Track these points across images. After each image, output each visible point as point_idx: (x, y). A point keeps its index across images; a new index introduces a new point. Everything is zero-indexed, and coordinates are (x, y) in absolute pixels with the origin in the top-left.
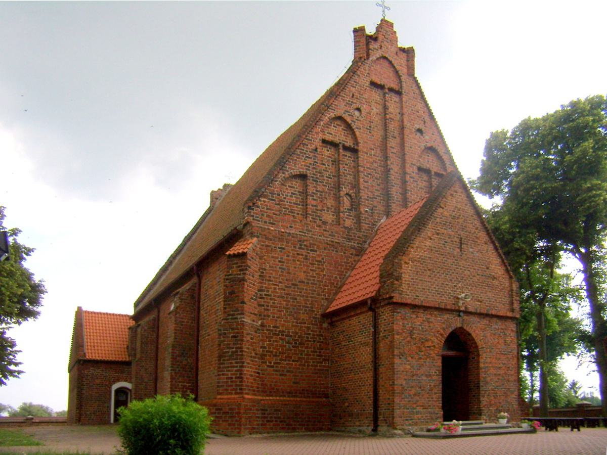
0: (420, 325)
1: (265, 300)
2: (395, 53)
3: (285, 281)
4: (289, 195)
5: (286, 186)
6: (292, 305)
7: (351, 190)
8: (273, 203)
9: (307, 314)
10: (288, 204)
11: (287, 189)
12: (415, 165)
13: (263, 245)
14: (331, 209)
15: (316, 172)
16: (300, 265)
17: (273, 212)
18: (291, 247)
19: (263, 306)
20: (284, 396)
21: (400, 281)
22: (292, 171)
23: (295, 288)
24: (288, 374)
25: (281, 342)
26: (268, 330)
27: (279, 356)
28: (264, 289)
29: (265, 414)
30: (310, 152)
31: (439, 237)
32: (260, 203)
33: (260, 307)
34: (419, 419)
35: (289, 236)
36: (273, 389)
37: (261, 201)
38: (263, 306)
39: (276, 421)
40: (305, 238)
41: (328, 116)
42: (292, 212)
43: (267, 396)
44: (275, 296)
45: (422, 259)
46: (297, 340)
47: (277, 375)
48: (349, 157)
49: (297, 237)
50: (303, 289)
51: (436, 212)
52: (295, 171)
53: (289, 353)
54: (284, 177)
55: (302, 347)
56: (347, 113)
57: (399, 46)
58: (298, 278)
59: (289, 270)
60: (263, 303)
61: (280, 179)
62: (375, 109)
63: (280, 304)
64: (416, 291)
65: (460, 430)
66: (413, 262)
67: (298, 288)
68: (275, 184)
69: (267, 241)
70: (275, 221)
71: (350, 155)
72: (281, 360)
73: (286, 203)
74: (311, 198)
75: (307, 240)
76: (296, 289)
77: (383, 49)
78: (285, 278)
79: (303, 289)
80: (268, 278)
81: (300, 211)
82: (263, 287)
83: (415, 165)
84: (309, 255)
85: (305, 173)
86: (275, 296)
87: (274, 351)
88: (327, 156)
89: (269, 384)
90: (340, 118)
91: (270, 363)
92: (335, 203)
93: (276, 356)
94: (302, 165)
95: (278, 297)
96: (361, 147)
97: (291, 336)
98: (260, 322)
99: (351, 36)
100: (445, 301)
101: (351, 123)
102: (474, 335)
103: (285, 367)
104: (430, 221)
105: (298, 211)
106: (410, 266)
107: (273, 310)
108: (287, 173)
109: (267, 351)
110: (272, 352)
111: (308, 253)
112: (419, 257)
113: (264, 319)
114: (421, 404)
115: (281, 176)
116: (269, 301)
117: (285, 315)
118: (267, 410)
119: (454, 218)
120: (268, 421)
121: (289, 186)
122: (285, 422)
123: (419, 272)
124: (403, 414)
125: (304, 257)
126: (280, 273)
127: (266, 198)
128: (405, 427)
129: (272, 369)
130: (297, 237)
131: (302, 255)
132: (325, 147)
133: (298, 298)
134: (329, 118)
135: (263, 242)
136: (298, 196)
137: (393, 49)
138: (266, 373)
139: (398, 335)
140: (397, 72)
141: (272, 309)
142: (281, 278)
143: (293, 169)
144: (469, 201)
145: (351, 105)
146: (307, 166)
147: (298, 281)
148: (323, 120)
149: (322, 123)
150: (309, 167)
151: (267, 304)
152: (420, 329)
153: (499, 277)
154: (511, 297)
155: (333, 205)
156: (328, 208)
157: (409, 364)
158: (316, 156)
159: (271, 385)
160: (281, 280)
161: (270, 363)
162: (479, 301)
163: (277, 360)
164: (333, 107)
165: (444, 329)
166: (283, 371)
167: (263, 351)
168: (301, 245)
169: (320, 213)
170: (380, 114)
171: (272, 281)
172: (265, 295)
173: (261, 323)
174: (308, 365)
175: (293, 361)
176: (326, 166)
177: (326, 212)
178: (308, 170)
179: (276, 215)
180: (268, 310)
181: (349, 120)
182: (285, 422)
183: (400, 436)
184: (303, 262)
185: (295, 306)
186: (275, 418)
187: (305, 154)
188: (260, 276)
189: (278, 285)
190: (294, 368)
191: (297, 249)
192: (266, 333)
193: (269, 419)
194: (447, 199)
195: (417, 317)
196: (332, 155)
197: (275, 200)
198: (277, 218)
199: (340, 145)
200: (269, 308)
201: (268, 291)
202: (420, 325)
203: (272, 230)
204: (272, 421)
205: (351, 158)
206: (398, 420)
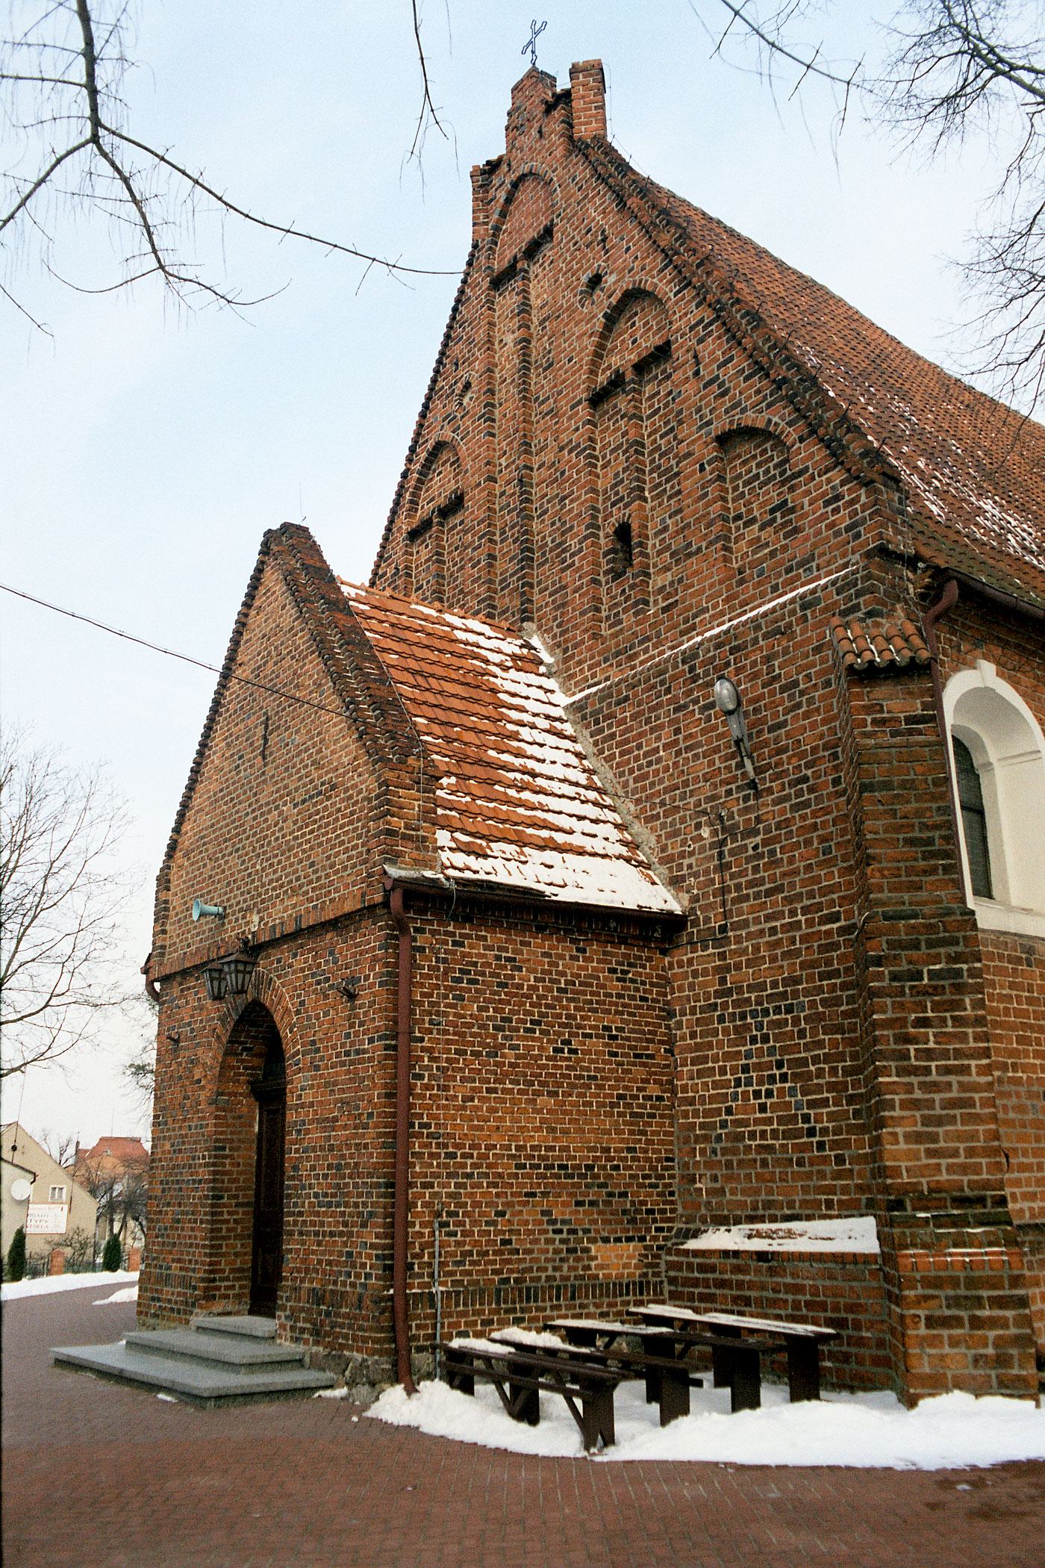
99: (468, 186)
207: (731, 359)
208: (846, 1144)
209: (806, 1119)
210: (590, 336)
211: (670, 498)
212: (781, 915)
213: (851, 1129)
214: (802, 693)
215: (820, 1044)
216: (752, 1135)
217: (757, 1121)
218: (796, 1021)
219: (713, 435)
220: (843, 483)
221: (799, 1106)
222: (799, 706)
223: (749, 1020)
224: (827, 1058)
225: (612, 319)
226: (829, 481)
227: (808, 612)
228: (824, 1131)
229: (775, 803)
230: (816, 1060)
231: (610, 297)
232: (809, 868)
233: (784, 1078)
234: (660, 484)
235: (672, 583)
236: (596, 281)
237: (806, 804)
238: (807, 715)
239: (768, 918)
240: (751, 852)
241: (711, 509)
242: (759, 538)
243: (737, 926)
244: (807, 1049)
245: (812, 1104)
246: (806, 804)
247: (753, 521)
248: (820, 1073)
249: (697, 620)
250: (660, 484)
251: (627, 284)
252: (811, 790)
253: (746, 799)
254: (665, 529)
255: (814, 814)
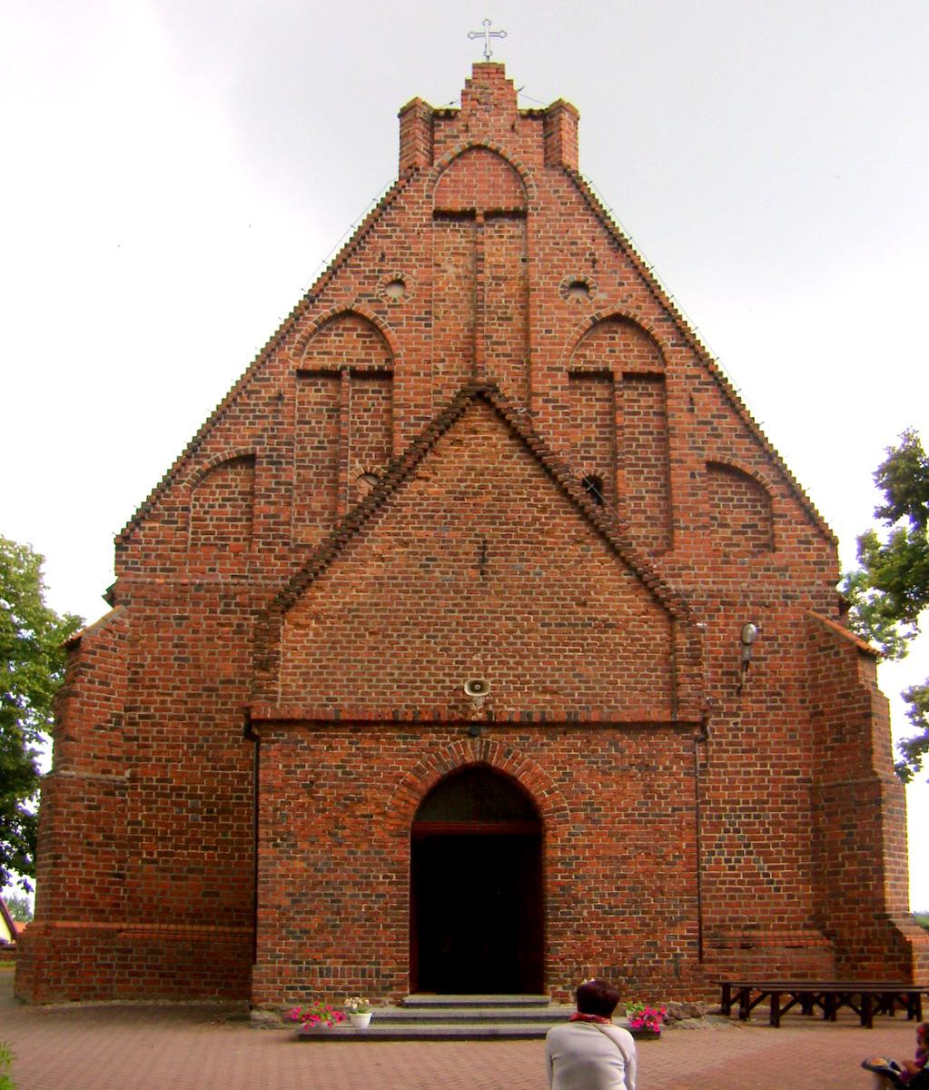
0: (338, 767)
1: (141, 727)
2: (508, 127)
3: (188, 684)
4: (217, 504)
5: (210, 486)
6: (201, 733)
7: (377, 462)
8: (171, 529)
9: (239, 747)
10: (215, 522)
11: (213, 493)
12: (560, 369)
13: (139, 618)
14: (323, 514)
15: (278, 444)
16: (224, 646)
17: (169, 546)
18: (204, 612)
19: (136, 739)
20: (182, 922)
21: (272, 670)
22: (218, 454)
23: (211, 696)
24: (191, 876)
25: (175, 810)
26: (144, 788)
27: (170, 839)
28: (138, 704)
29: (125, 959)
30: (264, 404)
31: (410, 549)
32: (142, 533)
33: (130, 743)
34: (328, 988)
35: (199, 590)
36: (156, 907)
37: (143, 529)
38: (136, 739)
39: (150, 975)
40: (239, 588)
41: (316, 317)
42: (223, 539)
43: (141, 921)
44: (163, 717)
45: (350, 610)
46: (215, 804)
47: (163, 878)
48: (373, 392)
49: (218, 591)
50: (231, 696)
51: (401, 493)
52: (226, 452)
53: (195, 833)
54: (199, 471)
55: (227, 819)
56: (364, 300)
57: (524, 104)
58: (218, 675)
59: (198, 660)
60: (135, 734)
61: (189, 477)
62: (451, 270)
63: (175, 732)
64: (327, 687)
65: (365, 1021)
66: (318, 621)
67: (217, 696)
68: (179, 489)
69: (148, 608)
70: (176, 564)
71: (377, 388)
72: (176, 847)
73: (208, 522)
74: (263, 501)
75: (242, 593)
76: (214, 699)
77: (474, 131)
78: (188, 679)
79: (231, 696)
80: (147, 683)
81: (241, 533)
82: (135, 701)
83: (560, 369)
84: (245, 623)
85: (250, 452)
86: (163, 717)
87: (160, 828)
88: (316, 403)
89: (145, 898)
90: (349, 314)
91: (150, 854)
92: (330, 501)
93: (163, 839)
94: (243, 437)
95: (171, 718)
96: (400, 364)
97: (200, 797)
98: (127, 773)
99: (395, 126)
100: (425, 700)
101: (377, 318)
102: (525, 779)
103: (185, 863)
104: (381, 516)
105: (235, 533)
106: (311, 633)
107: (159, 745)
108: (206, 461)
109: (143, 831)
110: (154, 832)
111: (245, 619)
112: (340, 607)
113: (137, 766)
114: (340, 953)
115: (192, 470)
116: (150, 728)
117: (185, 754)
118: (130, 951)
119: (461, 497)
120: (132, 974)
121: (217, 486)
122: (173, 976)
123: (340, 642)
124: (280, 974)
125: (235, 628)
126: (177, 669)
127: (155, 521)
128: (285, 1005)
129: (154, 866)
130: (218, 591)
131: (230, 625)
132: (310, 385)
133: (218, 716)
134: (316, 322)
135: (139, 611)
136: (240, 502)
137: (504, 121)
138: (139, 875)
139: (269, 792)
140: (513, 168)
141: (155, 744)
142: (177, 679)
143: (222, 450)
144: (518, 445)
145: (378, 277)
146: (255, 436)
147: (218, 679)
148: (299, 331)
149: (298, 336)
150: (261, 437)
151: (146, 735)
152: (340, 775)
153: (627, 621)
154: (672, 669)
155: (328, 504)
156: (314, 513)
157: (303, 859)
158: (278, 411)
159: (150, 899)
160: (178, 684)
161: (150, 854)
162: (546, 691)
163: (167, 847)
164: (327, 295)
165: (418, 770)
166: (180, 870)
167: (133, 831)
168: (227, 605)
169: (284, 530)
170: (466, 277)
171: (156, 687)
172: (141, 717)
173: (131, 774)
174: (241, 857)
175: (206, 848)
176: (313, 424)
177: (307, 523)
178: (259, 443)
179: (178, 551)
180: (146, 746)
181: (370, 312)
182: (173, 976)
183: (268, 1025)
184: (233, 639)
185: (211, 733)
186: (149, 967)
187: (254, 411)
188: (131, 680)
189: (171, 695)
190: (206, 863)
191: (219, 615)
192: (141, 793)
193: (135, 970)
194: (439, 455)
195: (330, 747)
196: (330, 397)
197: (176, 522)
198: (179, 557)
199: (343, 372)
200: (150, 742)
201: (147, 709)
202: (338, 767)
203: (160, 585)
204: (143, 974)
205: (380, 392)
206: (261, 987)
207: (725, 417)
208: (797, 889)
209: (766, 875)
210: (576, 325)
211: (646, 479)
212: (755, 765)
213: (799, 882)
214: (779, 645)
215: (781, 838)
216: (723, 883)
217: (725, 875)
218: (762, 824)
219: (705, 458)
220: (813, 536)
221: (760, 868)
222: (778, 652)
223: (724, 820)
224: (784, 845)
225: (597, 323)
226: (803, 530)
227: (789, 602)
228: (780, 882)
229: (753, 701)
230: (775, 845)
231: (599, 308)
232: (778, 743)
233: (750, 853)
234: (637, 465)
235: (646, 537)
236: (580, 285)
237: (779, 708)
238: (783, 659)
239: (743, 765)
240: (732, 725)
241: (700, 506)
242: (731, 539)
243: (713, 766)
244: (769, 838)
245: (769, 868)
246: (779, 708)
247: (727, 526)
248: (779, 853)
249: (683, 572)
250: (637, 465)
251: (619, 307)
252: (782, 701)
253: (730, 694)
254: (642, 498)
255: (785, 715)
